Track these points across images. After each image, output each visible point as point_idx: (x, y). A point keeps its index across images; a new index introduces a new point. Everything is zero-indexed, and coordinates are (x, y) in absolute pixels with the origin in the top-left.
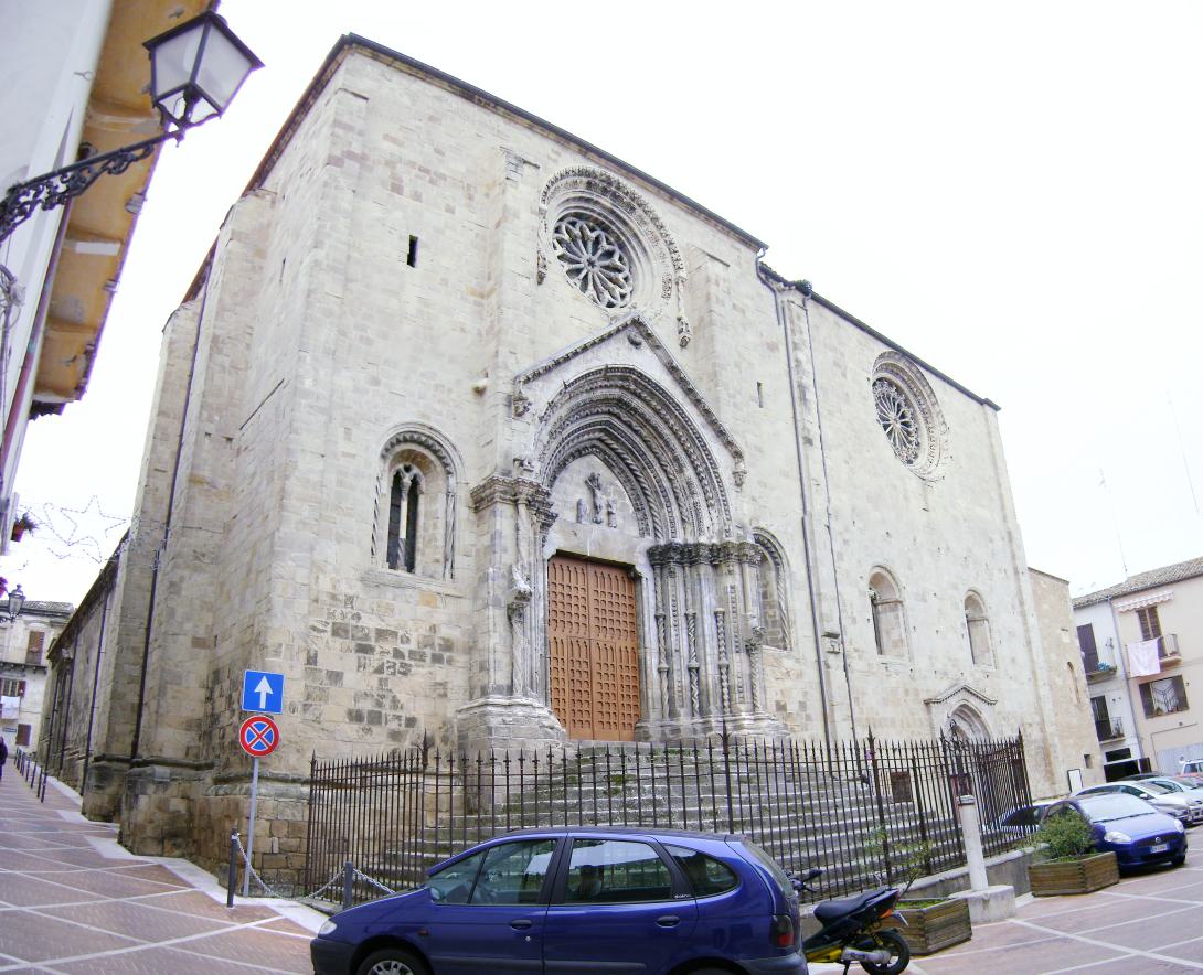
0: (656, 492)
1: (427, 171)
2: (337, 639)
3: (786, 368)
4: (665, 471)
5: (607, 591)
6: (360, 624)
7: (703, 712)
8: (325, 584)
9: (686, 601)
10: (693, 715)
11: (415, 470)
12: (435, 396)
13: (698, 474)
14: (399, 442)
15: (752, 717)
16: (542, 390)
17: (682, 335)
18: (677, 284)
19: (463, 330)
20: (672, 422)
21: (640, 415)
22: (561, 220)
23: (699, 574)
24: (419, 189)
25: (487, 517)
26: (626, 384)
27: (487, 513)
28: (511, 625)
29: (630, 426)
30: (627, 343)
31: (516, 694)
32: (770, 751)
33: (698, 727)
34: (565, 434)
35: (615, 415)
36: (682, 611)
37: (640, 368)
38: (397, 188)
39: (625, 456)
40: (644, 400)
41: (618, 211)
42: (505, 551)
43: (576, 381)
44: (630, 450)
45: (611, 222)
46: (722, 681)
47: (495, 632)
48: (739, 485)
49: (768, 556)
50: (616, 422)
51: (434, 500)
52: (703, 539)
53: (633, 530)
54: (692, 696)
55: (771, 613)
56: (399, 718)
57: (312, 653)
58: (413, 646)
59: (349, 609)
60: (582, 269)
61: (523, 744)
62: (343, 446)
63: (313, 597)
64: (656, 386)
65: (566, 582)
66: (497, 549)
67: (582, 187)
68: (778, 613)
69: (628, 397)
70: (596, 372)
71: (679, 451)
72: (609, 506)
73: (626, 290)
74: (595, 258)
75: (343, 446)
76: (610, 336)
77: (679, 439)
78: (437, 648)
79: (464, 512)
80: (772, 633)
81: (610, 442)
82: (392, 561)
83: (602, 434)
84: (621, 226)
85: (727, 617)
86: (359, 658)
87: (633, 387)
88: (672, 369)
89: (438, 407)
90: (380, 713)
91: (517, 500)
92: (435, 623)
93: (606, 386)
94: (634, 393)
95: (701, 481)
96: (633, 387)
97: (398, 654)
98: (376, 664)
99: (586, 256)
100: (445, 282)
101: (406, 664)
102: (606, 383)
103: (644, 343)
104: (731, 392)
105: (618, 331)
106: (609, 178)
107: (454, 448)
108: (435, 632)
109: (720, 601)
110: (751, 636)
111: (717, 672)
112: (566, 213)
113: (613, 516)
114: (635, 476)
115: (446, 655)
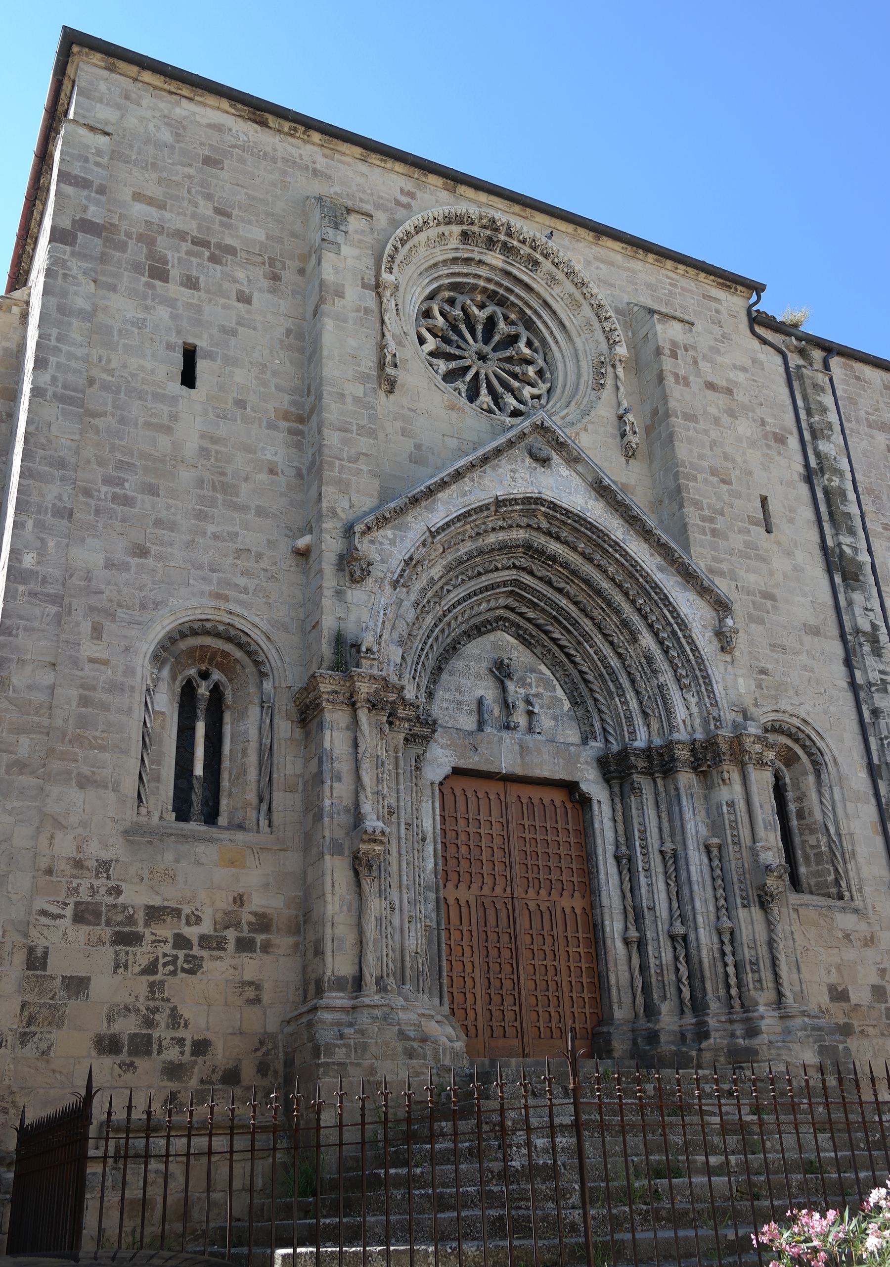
1: (205, 244)
2: (80, 926)
4: (611, 643)
6: (121, 900)
8: (65, 846)
9: (660, 830)
10: (682, 1012)
12: (236, 565)
13: (661, 643)
14: (183, 636)
15: (776, 1014)
16: (392, 542)
18: (614, 366)
20: (611, 570)
21: (561, 566)
22: (431, 297)
23: (677, 789)
24: (194, 273)
27: (313, 725)
28: (359, 884)
29: (549, 583)
30: (528, 461)
34: (446, 603)
35: (524, 569)
37: (548, 495)
38: (159, 273)
39: (549, 628)
40: (566, 543)
41: (515, 271)
42: (339, 779)
43: (448, 525)
44: (554, 617)
45: (508, 289)
46: (723, 954)
49: (800, 752)
50: (527, 579)
51: (242, 714)
52: (682, 735)
53: (572, 734)
54: (679, 980)
55: (812, 841)
56: (181, 1042)
57: (39, 952)
58: (206, 928)
59: (104, 881)
60: (469, 367)
61: (372, 1071)
62: (89, 649)
63: (43, 866)
64: (580, 519)
66: (327, 777)
67: (454, 242)
68: (824, 840)
69: (540, 540)
70: (480, 509)
71: (628, 610)
72: (528, 702)
74: (487, 349)
75: (89, 649)
76: (498, 452)
77: (626, 594)
78: (246, 928)
80: (818, 874)
81: (524, 610)
82: (182, 811)
84: (522, 293)
86: (117, 953)
87: (544, 525)
89: (242, 581)
90: (150, 1036)
92: (241, 891)
94: (549, 534)
97: (181, 942)
98: (144, 961)
99: (474, 346)
100: (241, 404)
101: (194, 957)
103: (555, 457)
104: (706, 512)
105: (511, 444)
106: (493, 221)
108: (242, 905)
109: (716, 827)
111: (716, 939)
112: (435, 285)
114: (568, 655)
115: (260, 938)
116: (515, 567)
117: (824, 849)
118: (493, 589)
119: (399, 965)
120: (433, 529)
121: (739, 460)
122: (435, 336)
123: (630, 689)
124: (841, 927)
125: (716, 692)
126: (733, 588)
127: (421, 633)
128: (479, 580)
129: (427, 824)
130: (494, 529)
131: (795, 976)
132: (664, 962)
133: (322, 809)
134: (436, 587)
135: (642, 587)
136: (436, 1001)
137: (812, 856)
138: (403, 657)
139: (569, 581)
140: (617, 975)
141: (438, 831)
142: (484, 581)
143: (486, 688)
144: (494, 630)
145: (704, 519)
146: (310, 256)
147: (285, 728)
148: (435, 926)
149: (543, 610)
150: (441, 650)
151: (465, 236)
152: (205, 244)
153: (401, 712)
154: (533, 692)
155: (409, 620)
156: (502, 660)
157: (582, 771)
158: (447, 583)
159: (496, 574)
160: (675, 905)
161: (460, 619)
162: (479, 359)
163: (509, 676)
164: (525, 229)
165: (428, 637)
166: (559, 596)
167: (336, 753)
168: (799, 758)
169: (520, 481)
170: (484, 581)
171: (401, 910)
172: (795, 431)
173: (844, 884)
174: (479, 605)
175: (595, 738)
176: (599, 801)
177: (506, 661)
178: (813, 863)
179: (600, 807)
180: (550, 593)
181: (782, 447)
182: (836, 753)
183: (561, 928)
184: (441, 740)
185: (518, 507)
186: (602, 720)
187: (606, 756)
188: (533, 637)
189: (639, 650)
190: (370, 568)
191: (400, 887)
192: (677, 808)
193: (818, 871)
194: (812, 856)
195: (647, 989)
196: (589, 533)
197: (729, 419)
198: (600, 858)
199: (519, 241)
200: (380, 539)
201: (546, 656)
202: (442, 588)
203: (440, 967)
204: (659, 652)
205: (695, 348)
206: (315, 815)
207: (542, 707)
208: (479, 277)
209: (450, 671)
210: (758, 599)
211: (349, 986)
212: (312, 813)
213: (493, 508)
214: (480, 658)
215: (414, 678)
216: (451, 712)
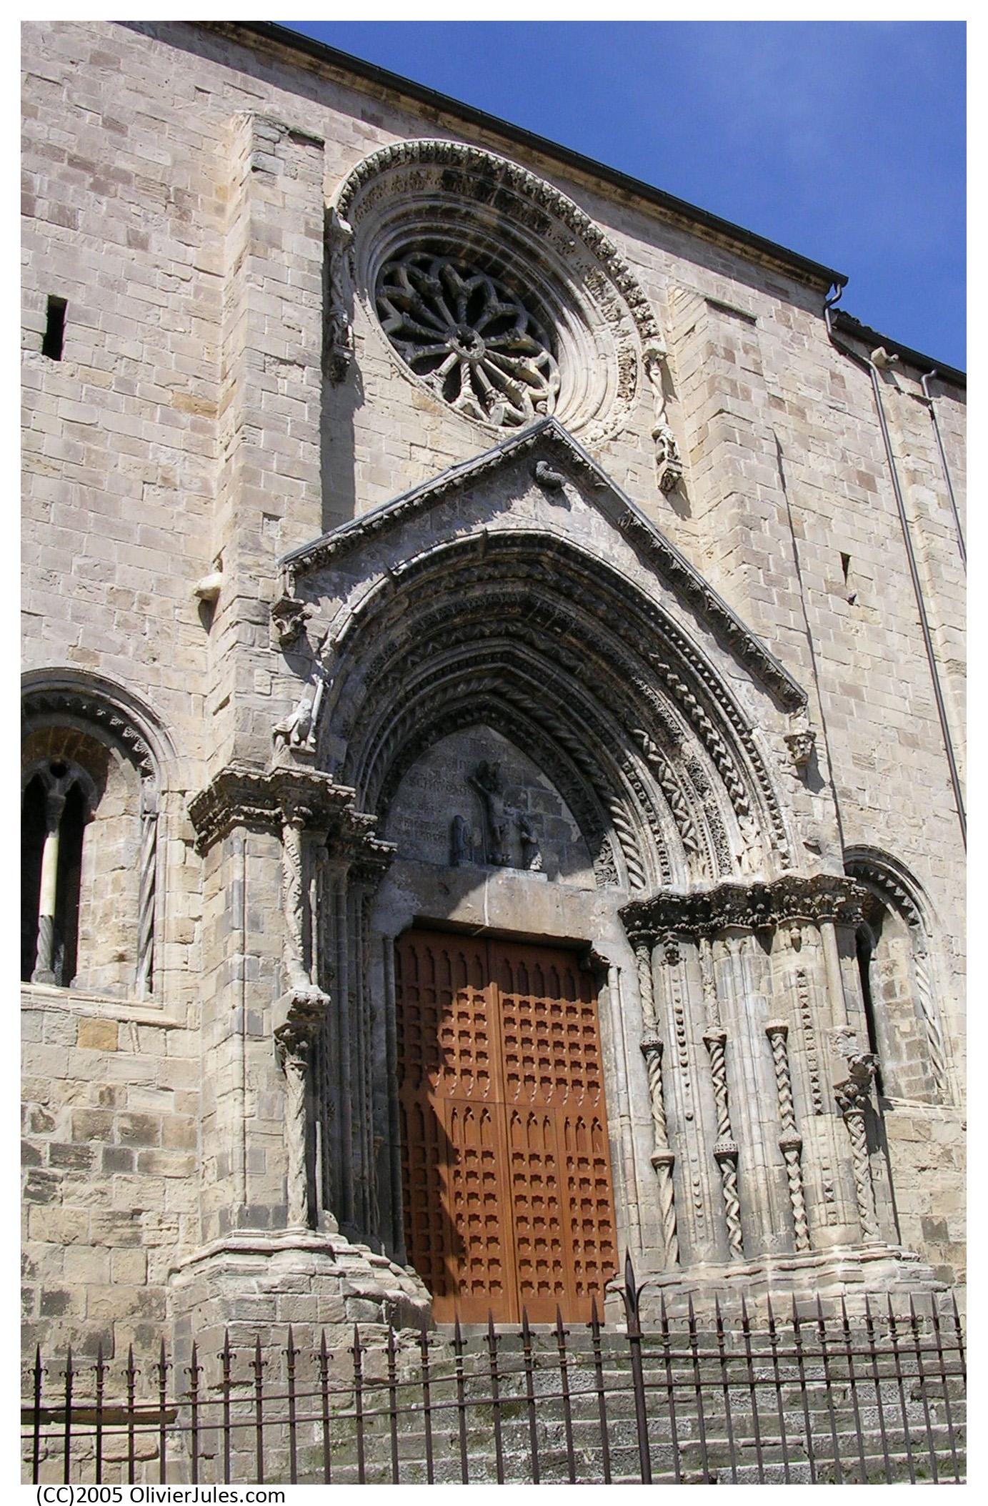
1: (87, 166)
11: (76, 773)
13: (709, 747)
17: (664, 465)
22: (397, 257)
24: (69, 204)
29: (556, 660)
32: (882, 1328)
35: (520, 638)
37: (564, 536)
50: (524, 653)
67: (432, 187)
73: (549, 388)
79: (175, 851)
81: (518, 696)
83: (498, 683)
88: (638, 537)
95: (716, 761)
100: (126, 387)
101: (45, 1177)
107: (155, 721)
115: (138, 1152)
116: (509, 635)
119: (338, 1193)
122: (400, 309)
129: (378, 997)
130: (480, 579)
132: (706, 1192)
138: (348, 756)
141: (393, 1006)
142: (464, 652)
144: (474, 723)
146: (235, 190)
148: (387, 1141)
151: (449, 181)
152: (87, 166)
154: (529, 812)
156: (487, 765)
157: (596, 925)
158: (411, 653)
161: (429, 705)
162: (461, 345)
163: (495, 789)
164: (530, 176)
165: (384, 728)
166: (568, 678)
169: (521, 512)
170: (464, 652)
174: (456, 686)
176: (619, 970)
177: (491, 769)
178: (905, 1056)
180: (555, 673)
184: (397, 876)
185: (516, 549)
188: (529, 734)
191: (341, 1083)
192: (729, 979)
193: (911, 1066)
196: (614, 591)
199: (522, 192)
200: (321, 583)
202: (404, 659)
203: (395, 1198)
204: (708, 760)
205: (757, 351)
207: (541, 835)
208: (464, 235)
211: (270, 1220)
214: (455, 763)
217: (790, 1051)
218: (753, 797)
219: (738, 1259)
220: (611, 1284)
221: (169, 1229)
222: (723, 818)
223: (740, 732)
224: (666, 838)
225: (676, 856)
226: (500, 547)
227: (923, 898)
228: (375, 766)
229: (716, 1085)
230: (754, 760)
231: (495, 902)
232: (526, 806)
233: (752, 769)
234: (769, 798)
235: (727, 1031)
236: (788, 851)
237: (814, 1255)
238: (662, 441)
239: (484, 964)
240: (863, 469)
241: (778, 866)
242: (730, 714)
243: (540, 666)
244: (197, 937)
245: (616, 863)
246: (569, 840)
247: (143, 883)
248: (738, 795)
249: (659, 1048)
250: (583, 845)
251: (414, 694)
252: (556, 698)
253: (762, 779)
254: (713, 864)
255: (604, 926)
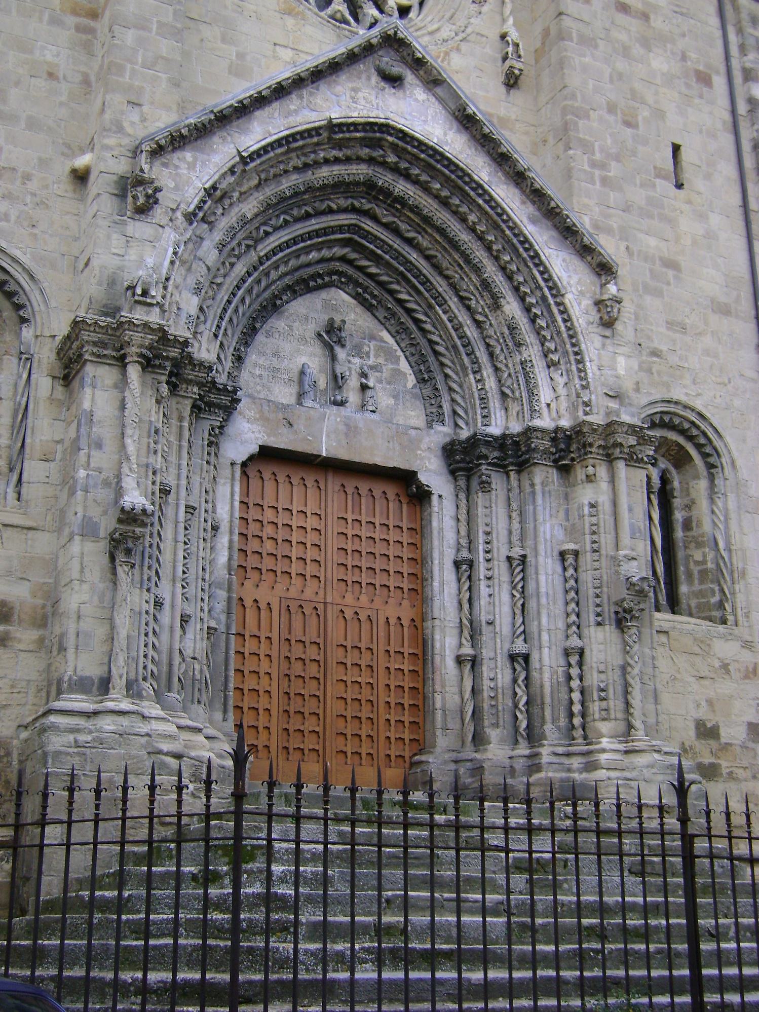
0: (455, 347)
3: (727, 117)
4: (468, 308)
5: (364, 519)
7: (533, 737)
9: (510, 532)
13: (528, 309)
15: (621, 747)
17: (508, 63)
19: (51, 75)
20: (472, 218)
21: (411, 210)
23: (532, 485)
25: (76, 390)
26: (379, 153)
27: (76, 383)
28: (114, 572)
29: (396, 232)
30: (375, 78)
31: (113, 694)
33: (519, 764)
36: (501, 550)
37: (400, 122)
40: (416, 182)
42: (99, 446)
43: (265, 149)
44: (401, 274)
46: (569, 678)
47: (82, 581)
48: (608, 323)
49: (693, 452)
50: (369, 225)
52: (545, 422)
53: (415, 416)
55: (698, 556)
64: (436, 154)
65: (269, 500)
66: (83, 443)
68: (711, 556)
69: (385, 179)
71: (491, 270)
77: (489, 248)
80: (701, 594)
83: (346, 250)
85: (581, 558)
87: (392, 159)
91: (124, 357)
93: (337, 161)
94: (395, 169)
95: (533, 321)
96: (392, 159)
102: (335, 153)
103: (410, 77)
104: (598, 156)
105: (352, 58)
107: (32, 277)
109: (572, 531)
110: (624, 593)
111: (562, 662)
113: (369, 393)
114: (417, 321)
117: (710, 565)
118: (326, 234)
120: (245, 154)
121: (650, 99)
123: (489, 365)
124: (719, 656)
125: (589, 371)
126: (622, 248)
127: (230, 282)
128: (308, 223)
131: (651, 707)
132: (500, 685)
133: (76, 482)
134: (251, 227)
135: (509, 242)
136: (219, 716)
137: (696, 573)
139: (420, 230)
140: (443, 699)
142: (314, 224)
143: (312, 355)
145: (593, 164)
147: (43, 384)
148: (223, 630)
149: (388, 265)
150: (256, 306)
153: (189, 373)
155: (210, 264)
159: (330, 217)
160: (519, 620)
163: (341, 343)
165: (238, 287)
167: (98, 415)
168: (690, 458)
169: (363, 102)
170: (314, 224)
171: (173, 606)
172: (722, 69)
173: (728, 607)
175: (443, 422)
176: (440, 496)
178: (696, 581)
179: (440, 503)
180: (397, 244)
181: (705, 89)
182: (735, 454)
183: (382, 640)
184: (247, 412)
185: (358, 135)
186: (453, 400)
187: (452, 443)
188: (374, 297)
189: (501, 318)
190: (159, 195)
192: (531, 508)
193: (701, 591)
194: (696, 573)
195: (477, 714)
197: (642, 51)
198: (436, 562)
201: (389, 320)
204: (525, 320)
206: (70, 488)
209: (267, 332)
210: (658, 267)
211: (95, 688)
212: (67, 487)
213: (325, 135)
214: (307, 318)
215: (216, 336)
216: (265, 381)
217: (580, 570)
218: (563, 353)
219: (523, 743)
220: (416, 757)
221: (19, 692)
222: (537, 370)
223: (554, 296)
224: (487, 387)
225: (495, 403)
226: (343, 132)
227: (723, 447)
228: (231, 320)
229: (514, 596)
230: (565, 321)
231: (333, 436)
232: (369, 357)
233: (563, 328)
234: (576, 354)
235: (528, 552)
236: (590, 400)
237: (587, 744)
238: (507, 41)
239: (322, 487)
240: (701, 68)
241: (581, 413)
242: (546, 280)
243: (382, 237)
244: (59, 456)
245: (445, 407)
246: (405, 386)
247: (16, 412)
248: (549, 351)
249: (471, 564)
250: (418, 391)
251: (268, 259)
252: (397, 266)
253: (571, 337)
254: (525, 409)
255: (429, 459)
